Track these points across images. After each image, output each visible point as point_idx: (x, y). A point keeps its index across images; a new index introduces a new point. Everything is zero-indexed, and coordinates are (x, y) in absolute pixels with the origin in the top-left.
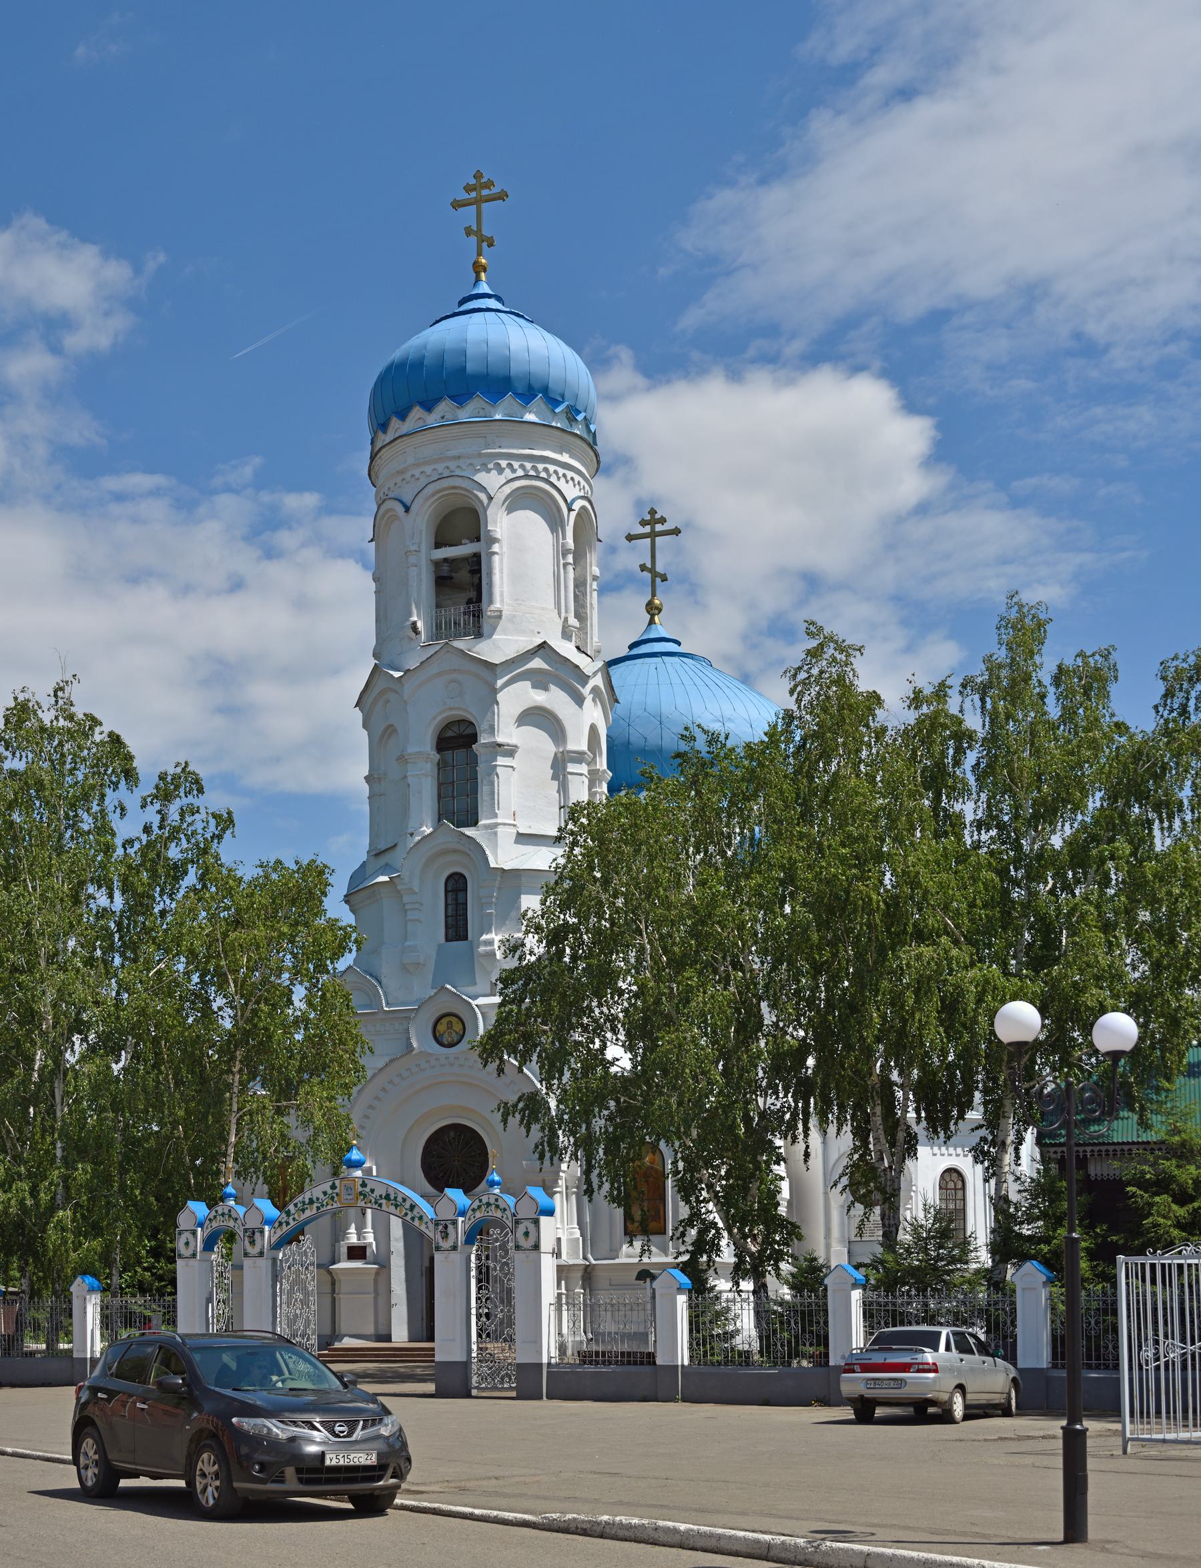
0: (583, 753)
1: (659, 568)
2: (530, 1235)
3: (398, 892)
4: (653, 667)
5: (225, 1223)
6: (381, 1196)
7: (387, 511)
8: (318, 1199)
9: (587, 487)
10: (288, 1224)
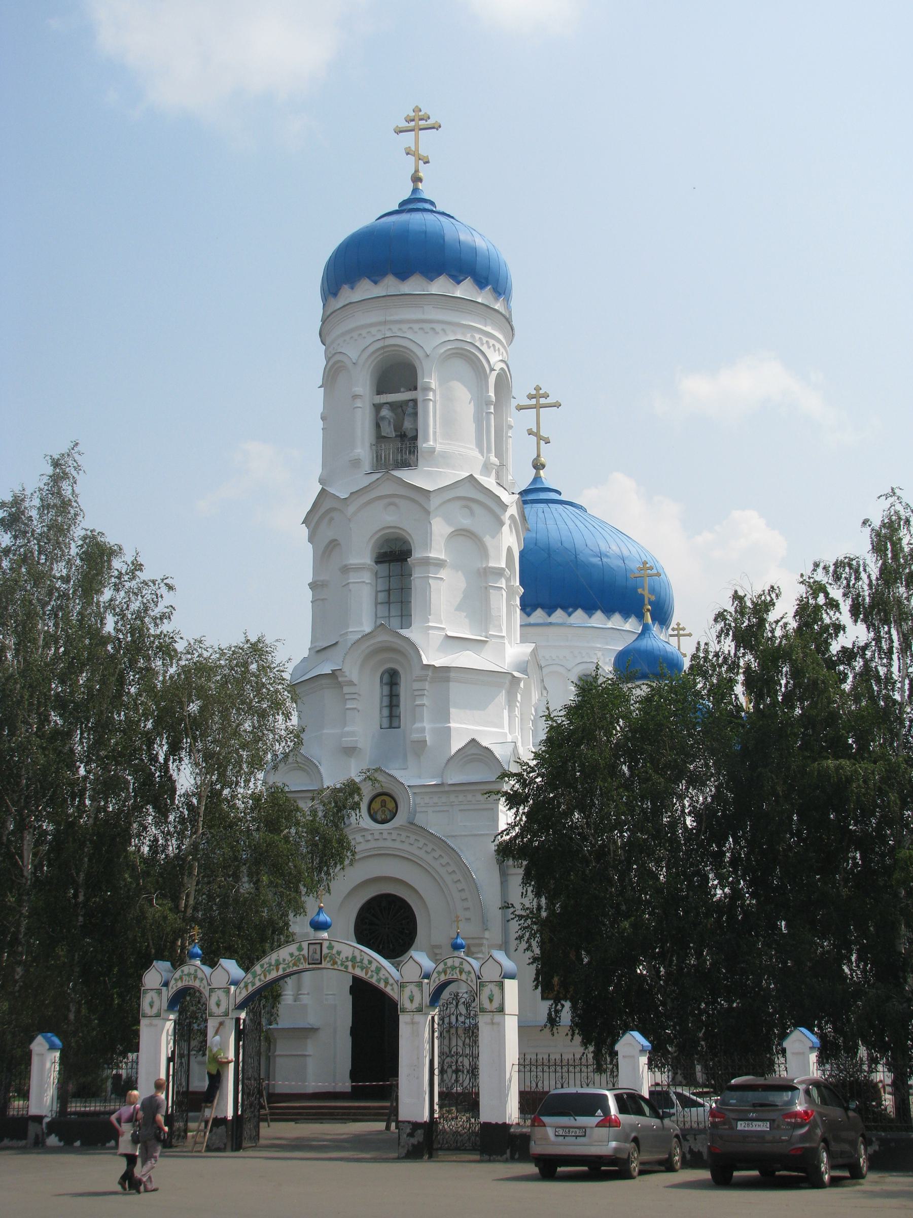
0: (503, 569)
1: (543, 433)
3: (339, 683)
4: (540, 511)
6: (347, 958)
8: (284, 960)
9: (505, 354)
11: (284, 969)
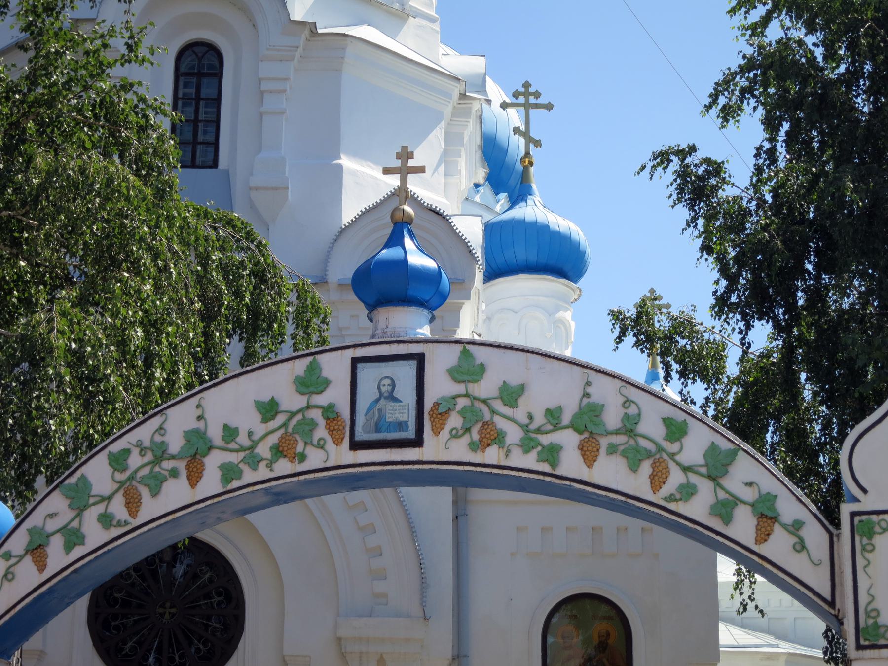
1: (533, 134)
6: (553, 415)
10: (73, 537)
11: (229, 472)
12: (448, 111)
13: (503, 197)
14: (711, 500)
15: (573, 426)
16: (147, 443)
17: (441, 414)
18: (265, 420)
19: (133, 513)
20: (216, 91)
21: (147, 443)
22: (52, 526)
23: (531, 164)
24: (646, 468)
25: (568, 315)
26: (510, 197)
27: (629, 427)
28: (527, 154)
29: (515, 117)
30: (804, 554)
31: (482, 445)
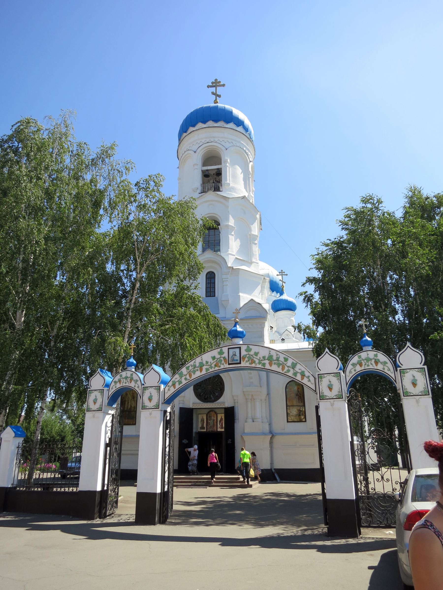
2: (153, 398)
5: (127, 384)
6: (264, 357)
7: (188, 154)
10: (180, 382)
11: (207, 370)
12: (261, 282)
13: (279, 294)
14: (293, 372)
15: (267, 359)
16: (192, 365)
17: (244, 358)
18: (213, 360)
19: (190, 378)
20: (214, 281)
21: (192, 365)
22: (176, 380)
23: (284, 287)
24: (281, 367)
25: (293, 318)
26: (280, 294)
27: (278, 359)
28: (283, 285)
29: (280, 277)
30: (310, 382)
31: (251, 363)
